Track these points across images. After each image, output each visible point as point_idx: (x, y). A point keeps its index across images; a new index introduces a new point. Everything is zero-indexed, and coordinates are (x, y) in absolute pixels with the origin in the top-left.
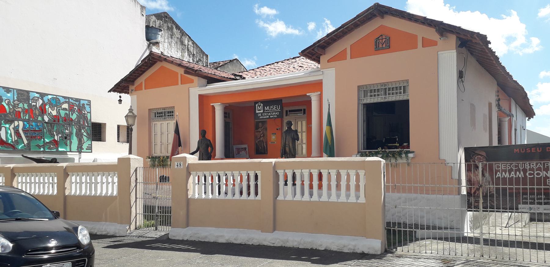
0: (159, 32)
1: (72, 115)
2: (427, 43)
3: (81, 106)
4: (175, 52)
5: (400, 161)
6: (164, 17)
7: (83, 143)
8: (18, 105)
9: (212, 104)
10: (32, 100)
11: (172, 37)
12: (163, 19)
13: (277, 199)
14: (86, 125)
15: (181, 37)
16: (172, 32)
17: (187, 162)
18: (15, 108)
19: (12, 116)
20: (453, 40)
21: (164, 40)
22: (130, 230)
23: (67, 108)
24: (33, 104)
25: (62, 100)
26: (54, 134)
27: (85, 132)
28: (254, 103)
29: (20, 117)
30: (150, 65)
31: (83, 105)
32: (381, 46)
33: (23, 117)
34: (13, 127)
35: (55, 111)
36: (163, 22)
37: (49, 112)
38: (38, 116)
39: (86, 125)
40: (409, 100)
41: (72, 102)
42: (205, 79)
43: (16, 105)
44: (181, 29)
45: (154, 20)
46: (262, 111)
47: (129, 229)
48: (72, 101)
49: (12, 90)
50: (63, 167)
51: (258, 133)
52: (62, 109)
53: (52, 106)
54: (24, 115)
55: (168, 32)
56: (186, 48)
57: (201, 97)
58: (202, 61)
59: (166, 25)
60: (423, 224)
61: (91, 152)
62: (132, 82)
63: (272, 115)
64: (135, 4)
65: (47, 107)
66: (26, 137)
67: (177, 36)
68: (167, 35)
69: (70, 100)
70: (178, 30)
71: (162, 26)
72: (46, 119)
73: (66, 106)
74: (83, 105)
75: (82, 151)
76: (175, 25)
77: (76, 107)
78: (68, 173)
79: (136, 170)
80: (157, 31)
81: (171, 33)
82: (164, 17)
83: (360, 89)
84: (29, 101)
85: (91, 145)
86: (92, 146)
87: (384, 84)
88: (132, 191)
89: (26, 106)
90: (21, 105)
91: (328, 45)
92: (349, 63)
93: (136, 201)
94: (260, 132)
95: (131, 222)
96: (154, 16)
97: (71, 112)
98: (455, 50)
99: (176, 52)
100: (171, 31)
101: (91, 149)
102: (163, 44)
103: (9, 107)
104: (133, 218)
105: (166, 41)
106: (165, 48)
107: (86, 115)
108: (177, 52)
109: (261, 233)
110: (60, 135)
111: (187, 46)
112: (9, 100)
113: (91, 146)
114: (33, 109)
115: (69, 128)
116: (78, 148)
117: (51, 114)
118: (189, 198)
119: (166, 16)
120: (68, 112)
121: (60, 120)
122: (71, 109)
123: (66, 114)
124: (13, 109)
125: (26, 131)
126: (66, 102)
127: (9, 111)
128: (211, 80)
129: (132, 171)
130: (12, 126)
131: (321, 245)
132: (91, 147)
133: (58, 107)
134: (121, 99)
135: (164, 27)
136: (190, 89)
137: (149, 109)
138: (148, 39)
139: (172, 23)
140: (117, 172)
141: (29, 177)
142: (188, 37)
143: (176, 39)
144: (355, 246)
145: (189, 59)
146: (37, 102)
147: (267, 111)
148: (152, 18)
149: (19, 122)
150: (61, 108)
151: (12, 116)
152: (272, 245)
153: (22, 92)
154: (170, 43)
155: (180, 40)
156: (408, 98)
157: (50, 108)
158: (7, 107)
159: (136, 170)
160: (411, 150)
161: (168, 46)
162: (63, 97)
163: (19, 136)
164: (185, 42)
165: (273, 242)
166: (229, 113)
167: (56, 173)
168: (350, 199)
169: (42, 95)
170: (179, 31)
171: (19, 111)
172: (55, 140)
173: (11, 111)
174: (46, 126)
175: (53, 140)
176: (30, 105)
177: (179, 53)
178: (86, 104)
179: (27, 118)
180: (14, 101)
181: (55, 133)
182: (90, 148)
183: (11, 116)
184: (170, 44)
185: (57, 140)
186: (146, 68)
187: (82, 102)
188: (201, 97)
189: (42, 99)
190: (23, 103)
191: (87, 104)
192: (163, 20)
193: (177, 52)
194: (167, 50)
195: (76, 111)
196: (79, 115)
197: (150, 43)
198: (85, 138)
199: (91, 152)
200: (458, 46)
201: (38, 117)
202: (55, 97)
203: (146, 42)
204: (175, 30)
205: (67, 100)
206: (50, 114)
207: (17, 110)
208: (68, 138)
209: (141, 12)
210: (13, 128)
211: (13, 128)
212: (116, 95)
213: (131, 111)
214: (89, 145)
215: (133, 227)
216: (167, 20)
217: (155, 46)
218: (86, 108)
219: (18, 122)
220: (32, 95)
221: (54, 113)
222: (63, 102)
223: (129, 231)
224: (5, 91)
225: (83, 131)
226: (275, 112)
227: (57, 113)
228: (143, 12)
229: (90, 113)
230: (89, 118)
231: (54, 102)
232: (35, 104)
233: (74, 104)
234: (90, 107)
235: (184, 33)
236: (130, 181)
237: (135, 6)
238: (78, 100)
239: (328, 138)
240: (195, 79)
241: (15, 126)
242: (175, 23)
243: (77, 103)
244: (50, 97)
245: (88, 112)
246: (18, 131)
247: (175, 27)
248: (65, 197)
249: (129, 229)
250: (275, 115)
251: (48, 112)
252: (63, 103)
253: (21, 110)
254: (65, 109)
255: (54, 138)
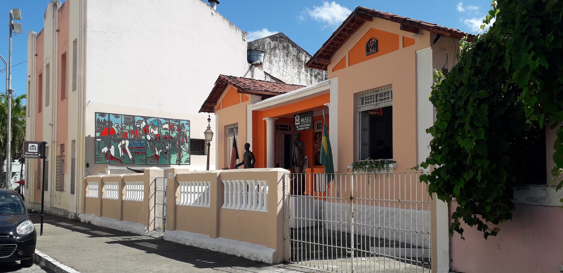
0: (261, 53)
1: (172, 133)
2: (407, 43)
3: (181, 125)
4: (291, 69)
5: (382, 172)
6: (280, 38)
7: (182, 157)
8: (125, 127)
9: (263, 119)
10: (137, 122)
11: (288, 55)
12: (279, 39)
13: (222, 207)
14: (185, 141)
15: (298, 54)
16: (288, 51)
17: (175, 173)
18: (122, 130)
19: (120, 137)
20: (427, 36)
21: (280, 59)
22: (148, 230)
23: (168, 127)
24: (138, 126)
25: (163, 121)
26: (155, 150)
27: (184, 147)
28: (294, 116)
29: (127, 137)
30: (224, 87)
31: (183, 124)
32: (371, 50)
33: (129, 136)
34: (121, 145)
35: (157, 131)
36: (278, 42)
37: (151, 132)
38: (142, 135)
39: (185, 141)
40: (392, 106)
41: (172, 123)
42: (259, 96)
43: (124, 128)
44: (298, 47)
45: (269, 42)
46: (299, 123)
47: (147, 230)
48: (173, 122)
49: (121, 116)
50: (121, 177)
51: (316, 144)
52: (163, 129)
53: (154, 127)
54: (130, 135)
55: (284, 51)
56: (303, 64)
57: (255, 113)
58: (321, 74)
59: (281, 44)
60: (382, 238)
61: (190, 164)
62: (215, 102)
63: (306, 127)
64: (236, 31)
65: (149, 128)
66: (131, 153)
67: (293, 53)
68: (282, 54)
69: (171, 121)
70: (294, 48)
71: (278, 46)
72: (149, 137)
73: (166, 126)
74: (183, 124)
75: (181, 163)
76: (291, 43)
77: (176, 127)
78: (179, 182)
79: (155, 180)
80: (259, 53)
81: (287, 52)
82: (280, 38)
83: (358, 96)
84: (134, 124)
85: (190, 158)
86: (190, 159)
87: (376, 90)
88: (151, 197)
89: (132, 128)
90: (128, 127)
91: (332, 54)
92: (348, 69)
93: (155, 206)
94: (317, 143)
95: (150, 224)
96: (268, 39)
97: (171, 131)
98: (431, 47)
99: (292, 69)
100: (287, 50)
101: (190, 162)
102: (279, 64)
103: (118, 129)
104: (152, 221)
105: (282, 60)
106: (280, 67)
107: (185, 133)
108: (293, 68)
109: (210, 238)
110: (161, 151)
111: (305, 62)
112: (117, 124)
113: (189, 159)
114: (138, 130)
115: (169, 144)
116: (177, 161)
117: (153, 134)
118: (177, 204)
119: (281, 37)
120: (168, 131)
121: (161, 138)
122: (171, 128)
123: (166, 132)
124: (121, 130)
125: (131, 148)
126: (167, 123)
127: (118, 133)
128: (264, 97)
129: (151, 180)
130: (120, 144)
131: (238, 252)
132: (190, 160)
133: (159, 127)
134: (210, 118)
135: (279, 47)
136: (247, 106)
137: (225, 126)
138: (250, 60)
139: (288, 41)
140: (209, 182)
141: (183, 186)
142: (305, 53)
143: (292, 57)
144: (257, 254)
145: (306, 73)
146: (141, 124)
147: (302, 122)
148: (266, 40)
149: (126, 141)
150: (162, 128)
151: (120, 136)
152: (213, 250)
153: (129, 117)
154: (286, 61)
155: (297, 57)
156: (391, 104)
157: (152, 129)
158: (116, 129)
159: (155, 180)
160: (394, 159)
161: (283, 64)
162: (164, 119)
163: (125, 152)
164: (302, 59)
165: (213, 247)
166: (290, 126)
167: (143, 182)
168: (257, 208)
169: (146, 118)
170: (296, 49)
171: (126, 132)
172: (156, 155)
173: (119, 133)
174: (148, 144)
175: (154, 155)
176: (135, 127)
177: (295, 69)
178: (185, 124)
179: (133, 137)
180: (122, 124)
181: (156, 149)
182: (188, 161)
183: (119, 137)
184: (286, 62)
185: (158, 154)
186: (222, 89)
187: (181, 122)
188: (255, 113)
189: (146, 122)
190: (129, 125)
191: (186, 124)
192: (278, 41)
193: (293, 68)
194: (283, 68)
195: (175, 130)
196: (178, 133)
197: (252, 65)
198: (184, 153)
199: (190, 164)
200: (432, 43)
201: (142, 136)
202: (157, 119)
203: (248, 64)
204: (291, 48)
205: (168, 121)
206: (152, 133)
207: (124, 131)
208: (134, 154)
209: (242, 38)
210: (120, 146)
211: (120, 146)
212: (206, 115)
213: (209, 128)
214: (187, 158)
215: (151, 228)
216: (283, 40)
217: (258, 67)
218: (185, 127)
219: (125, 141)
220: (137, 119)
221: (156, 132)
222: (164, 123)
223: (147, 231)
224: (114, 117)
225: (182, 147)
226: (308, 123)
227: (158, 132)
228: (244, 37)
229: (189, 131)
230: (188, 135)
231: (156, 124)
232: (139, 126)
233: (174, 124)
234: (189, 126)
235: (302, 50)
236: (149, 189)
237: (236, 33)
238: (177, 121)
239: (324, 149)
240: (249, 96)
241: (123, 144)
242: (291, 41)
243: (177, 123)
244: (152, 120)
245: (187, 131)
246: (125, 148)
247: (291, 46)
248: (122, 202)
249: (147, 230)
250: (307, 126)
251: (151, 132)
252: (164, 124)
253: (127, 132)
254: (166, 129)
255: (155, 153)
